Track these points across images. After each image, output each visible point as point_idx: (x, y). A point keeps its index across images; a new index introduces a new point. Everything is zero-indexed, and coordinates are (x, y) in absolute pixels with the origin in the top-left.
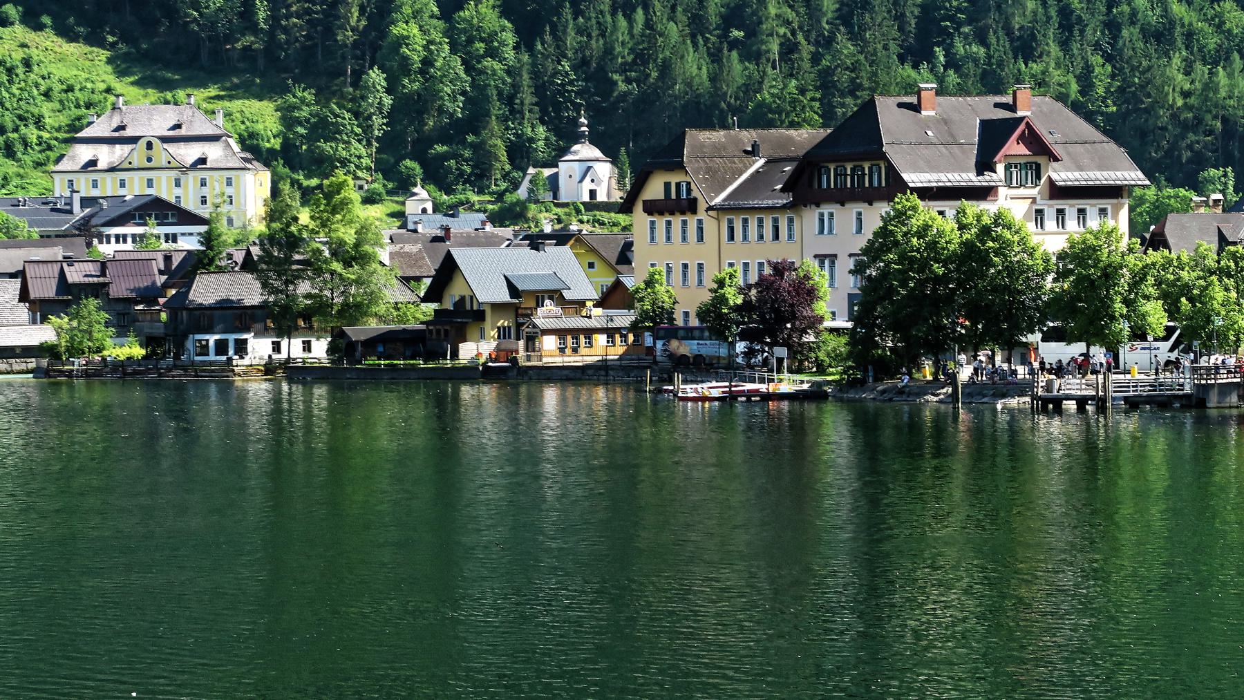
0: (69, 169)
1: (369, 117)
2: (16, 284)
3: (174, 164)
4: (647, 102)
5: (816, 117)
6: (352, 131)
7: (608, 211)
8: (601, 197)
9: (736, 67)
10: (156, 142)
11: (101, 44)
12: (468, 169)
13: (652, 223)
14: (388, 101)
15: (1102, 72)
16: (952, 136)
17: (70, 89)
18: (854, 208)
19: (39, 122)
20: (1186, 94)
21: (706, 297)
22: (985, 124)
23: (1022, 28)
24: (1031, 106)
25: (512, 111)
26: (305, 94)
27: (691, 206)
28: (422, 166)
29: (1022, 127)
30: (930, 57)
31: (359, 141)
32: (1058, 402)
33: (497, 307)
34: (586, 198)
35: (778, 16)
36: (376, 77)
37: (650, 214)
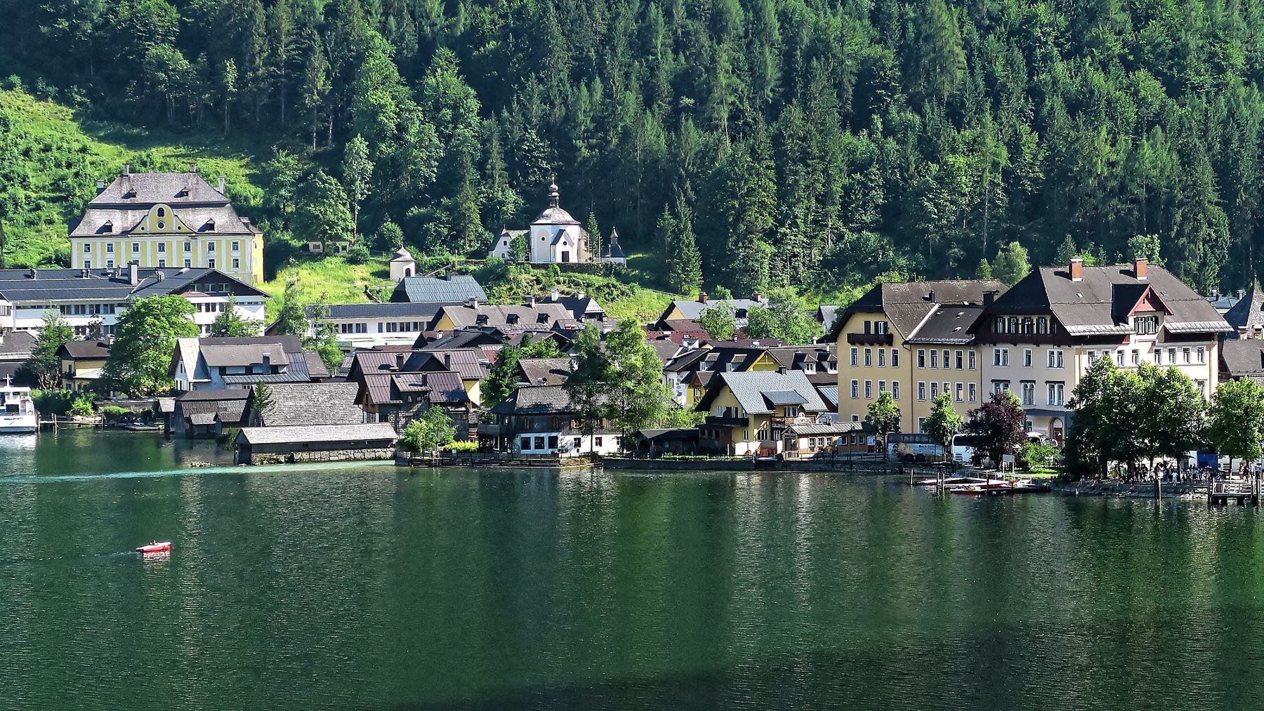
0: (86, 234)
1: (353, 182)
2: (354, 388)
3: (184, 229)
4: (606, 166)
5: (771, 184)
6: (339, 196)
7: (581, 272)
8: (573, 259)
9: (694, 137)
10: (167, 209)
11: (69, 102)
12: (445, 231)
13: (854, 350)
14: (370, 167)
15: (1030, 140)
16: (1095, 296)
17: (47, 149)
18: (1024, 348)
19: (24, 183)
20: (1112, 164)
21: (928, 414)
22: (1118, 289)
23: (951, 95)
24: (1148, 272)
25: (484, 176)
26: (289, 159)
27: (889, 340)
28: (403, 230)
29: (1147, 290)
30: (868, 124)
31: (344, 205)
32: (1224, 499)
33: (759, 417)
34: (559, 260)
35: (728, 85)
36: (360, 144)
37: (853, 344)
